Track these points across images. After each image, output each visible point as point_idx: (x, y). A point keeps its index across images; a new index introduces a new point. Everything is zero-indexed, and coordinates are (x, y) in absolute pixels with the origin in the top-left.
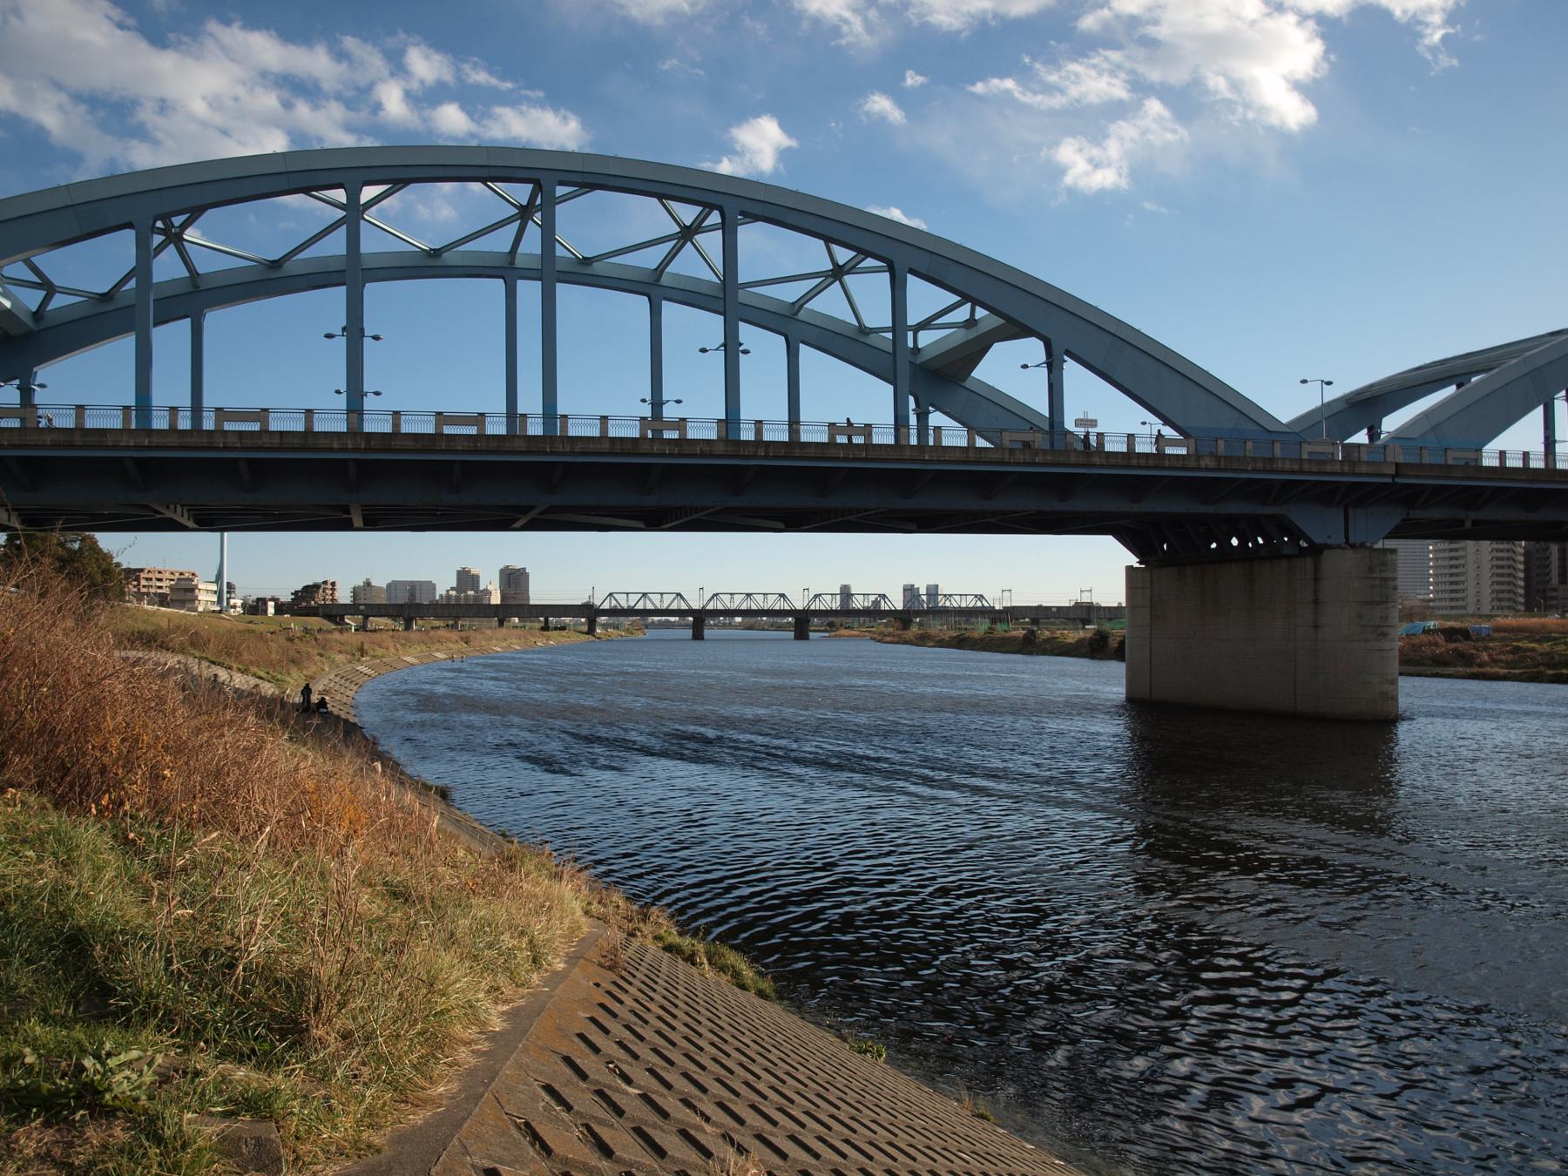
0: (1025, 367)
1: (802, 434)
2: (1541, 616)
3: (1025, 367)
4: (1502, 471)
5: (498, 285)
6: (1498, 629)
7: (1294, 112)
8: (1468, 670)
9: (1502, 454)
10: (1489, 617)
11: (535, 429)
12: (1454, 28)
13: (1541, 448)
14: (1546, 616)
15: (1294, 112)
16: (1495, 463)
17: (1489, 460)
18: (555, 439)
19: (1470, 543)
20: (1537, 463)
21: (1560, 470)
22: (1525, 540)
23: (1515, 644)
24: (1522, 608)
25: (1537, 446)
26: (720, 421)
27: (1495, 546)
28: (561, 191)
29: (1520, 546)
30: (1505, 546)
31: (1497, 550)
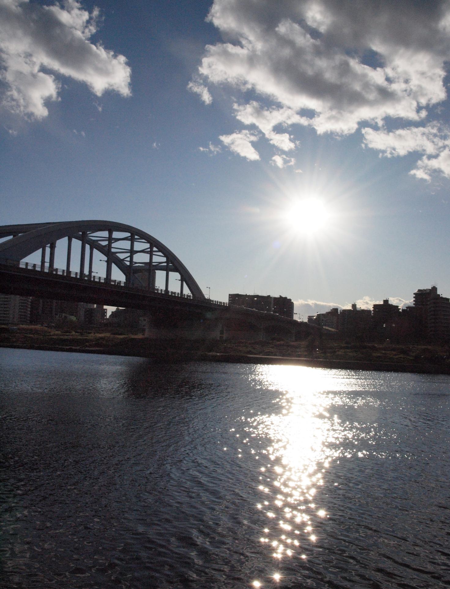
0: (101, 260)
1: (20, 265)
2: (34, 325)
3: (101, 260)
4: (26, 270)
5: (165, 272)
6: (19, 329)
7: (41, 111)
8: (8, 344)
9: (27, 264)
10: (16, 325)
11: (46, 270)
12: (361, 437)
13: (40, 264)
14: (36, 325)
15: (41, 111)
16: (24, 267)
17: (22, 266)
18: (50, 274)
19: (12, 296)
20: (38, 269)
21: (21, 268)
22: (97, 303)
23: (25, 335)
24: (29, 322)
25: (39, 263)
26: (105, 278)
27: (21, 298)
28: (136, 237)
29: (30, 299)
30: (24, 298)
31: (22, 300)
